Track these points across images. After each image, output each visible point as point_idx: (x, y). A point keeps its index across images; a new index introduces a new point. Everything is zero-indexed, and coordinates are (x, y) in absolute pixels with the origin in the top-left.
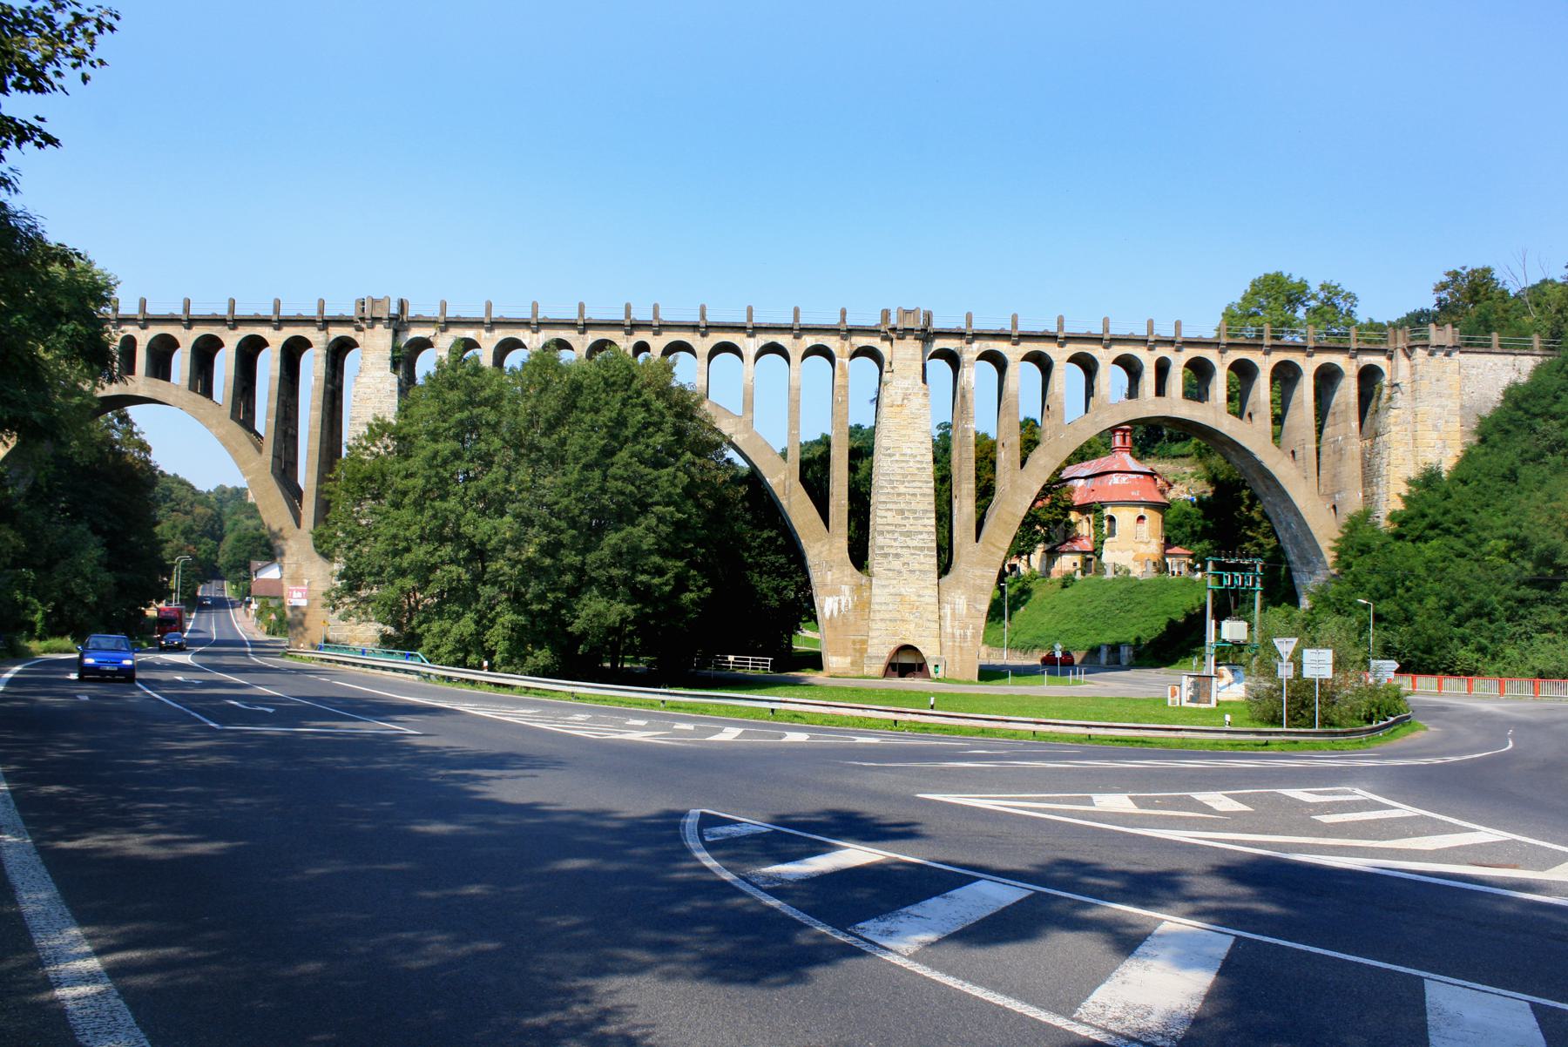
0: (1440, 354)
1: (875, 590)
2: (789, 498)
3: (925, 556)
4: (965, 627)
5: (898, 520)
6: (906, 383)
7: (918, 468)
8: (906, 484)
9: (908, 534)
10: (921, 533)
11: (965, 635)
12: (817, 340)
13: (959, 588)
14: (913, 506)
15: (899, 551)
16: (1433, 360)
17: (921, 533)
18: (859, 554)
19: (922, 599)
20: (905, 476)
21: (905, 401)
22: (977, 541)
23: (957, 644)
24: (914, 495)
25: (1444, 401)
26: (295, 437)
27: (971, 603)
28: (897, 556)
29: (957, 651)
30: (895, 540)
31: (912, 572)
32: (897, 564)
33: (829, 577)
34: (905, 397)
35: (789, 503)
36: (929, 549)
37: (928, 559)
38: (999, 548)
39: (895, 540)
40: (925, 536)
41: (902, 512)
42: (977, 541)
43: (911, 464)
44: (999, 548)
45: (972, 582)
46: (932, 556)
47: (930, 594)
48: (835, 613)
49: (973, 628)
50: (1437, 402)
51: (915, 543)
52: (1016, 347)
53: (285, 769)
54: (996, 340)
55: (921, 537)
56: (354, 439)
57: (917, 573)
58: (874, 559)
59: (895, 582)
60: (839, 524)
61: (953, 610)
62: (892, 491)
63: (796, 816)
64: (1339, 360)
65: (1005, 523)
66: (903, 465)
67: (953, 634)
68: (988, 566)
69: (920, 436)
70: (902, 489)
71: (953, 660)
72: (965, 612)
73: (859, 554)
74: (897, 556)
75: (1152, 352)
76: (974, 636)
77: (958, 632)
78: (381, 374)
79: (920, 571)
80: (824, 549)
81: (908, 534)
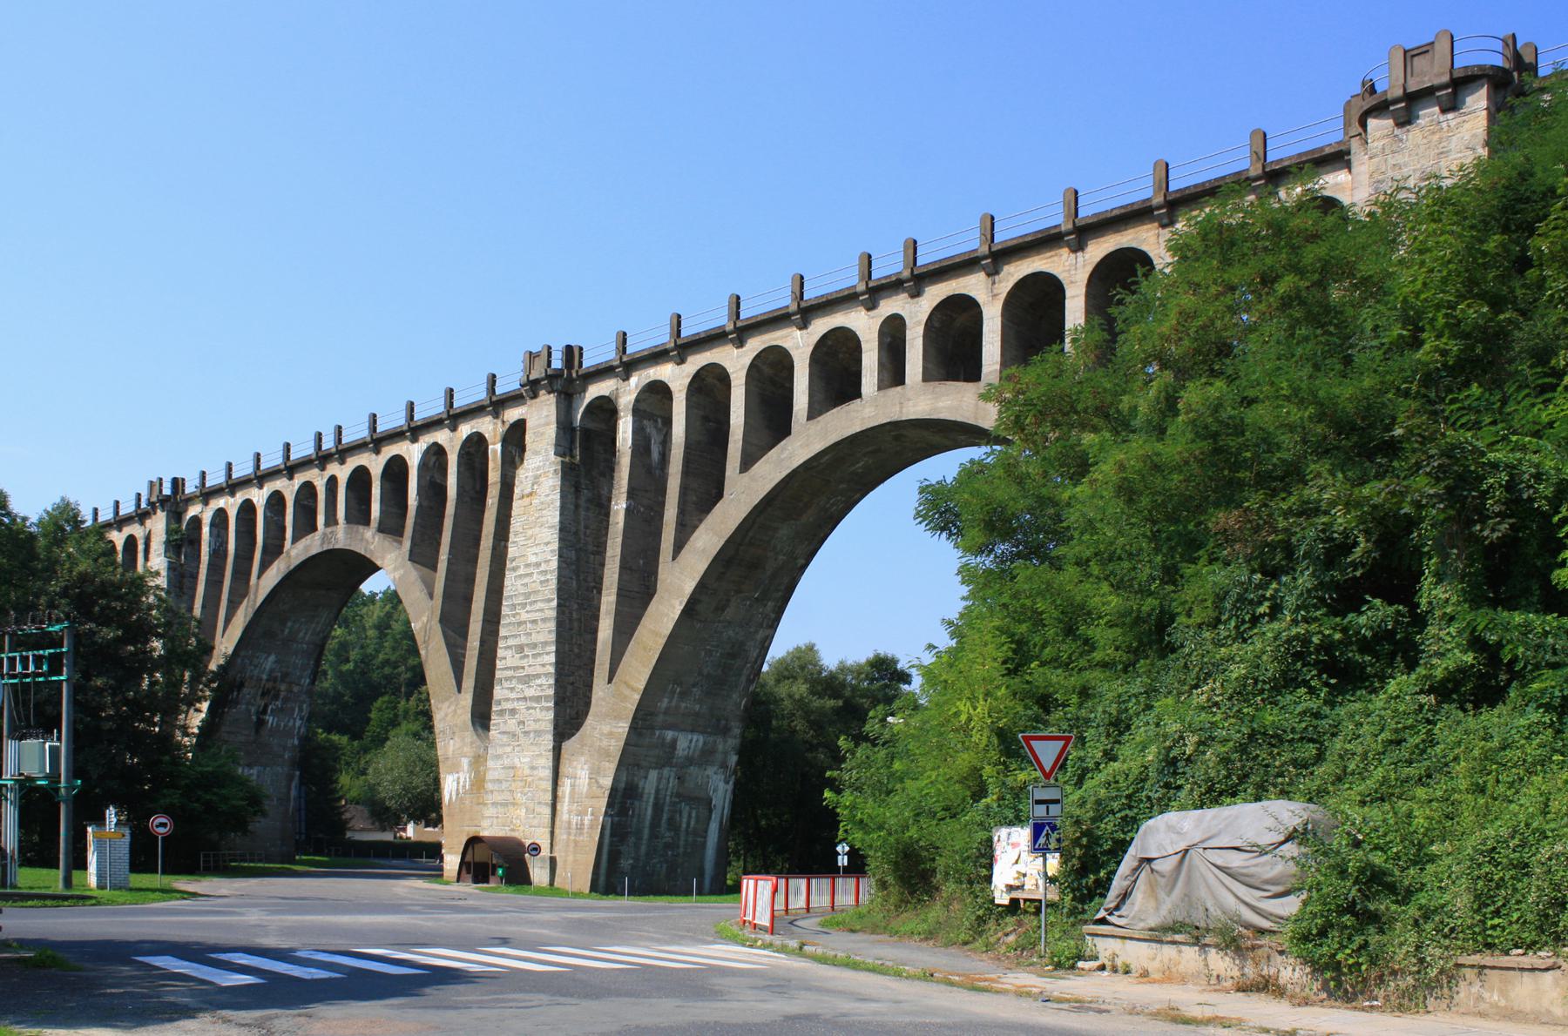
0: (1429, 114)
2: (427, 647)
3: (542, 709)
4: (581, 813)
7: (541, 582)
8: (528, 608)
10: (538, 676)
11: (582, 824)
12: (472, 427)
13: (582, 754)
15: (516, 705)
16: (1413, 135)
17: (538, 676)
18: (482, 716)
19: (535, 772)
20: (527, 595)
21: (535, 487)
22: (610, 681)
23: (572, 838)
24: (534, 622)
26: (485, 621)
27: (595, 773)
29: (572, 845)
30: (512, 689)
31: (526, 733)
33: (451, 749)
35: (427, 656)
36: (547, 698)
37: (544, 713)
38: (633, 689)
39: (512, 689)
40: (542, 681)
42: (610, 681)
43: (535, 577)
44: (633, 689)
45: (598, 744)
46: (548, 709)
48: (454, 798)
49: (592, 814)
51: (530, 692)
52: (683, 366)
54: (657, 363)
55: (538, 682)
57: (532, 735)
59: (509, 749)
61: (573, 786)
62: (513, 620)
63: (856, 1015)
65: (645, 649)
66: (526, 580)
67: (569, 823)
68: (618, 718)
70: (524, 616)
71: (566, 861)
72: (585, 790)
73: (482, 716)
74: (513, 712)
75: (872, 313)
76: (591, 827)
77: (575, 819)
79: (535, 731)
80: (450, 710)
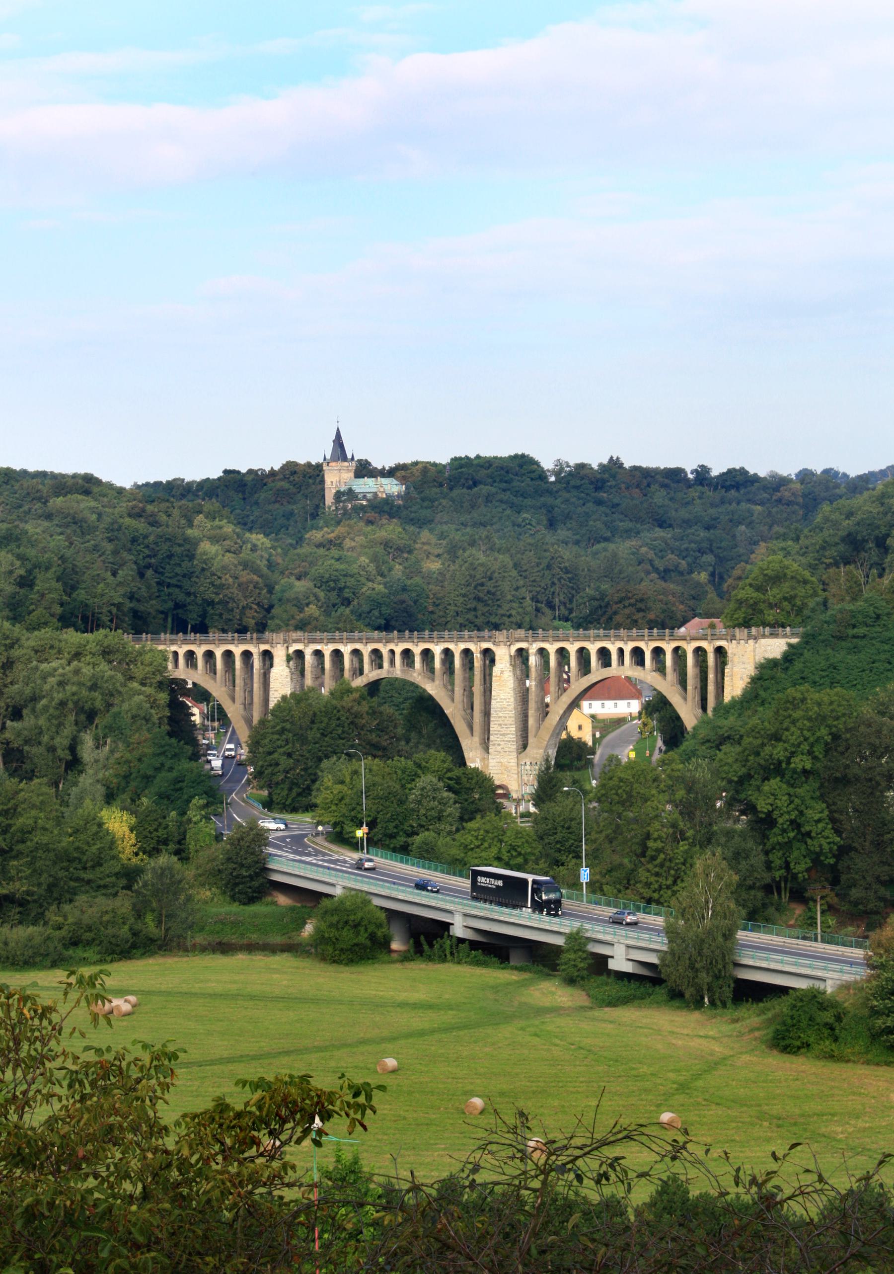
1: (490, 761)
5: (499, 728)
6: (502, 666)
9: (503, 735)
14: (506, 722)
25: (746, 666)
28: (499, 745)
32: (499, 748)
34: (502, 672)
41: (500, 725)
47: (513, 762)
50: (743, 666)
53: (182, 897)
56: (145, 1046)
58: (492, 749)
60: (503, 709)
64: (704, 644)
68: (539, 748)
69: (508, 690)
70: (501, 715)
74: (499, 745)
78: (282, 668)
81: (503, 735)
